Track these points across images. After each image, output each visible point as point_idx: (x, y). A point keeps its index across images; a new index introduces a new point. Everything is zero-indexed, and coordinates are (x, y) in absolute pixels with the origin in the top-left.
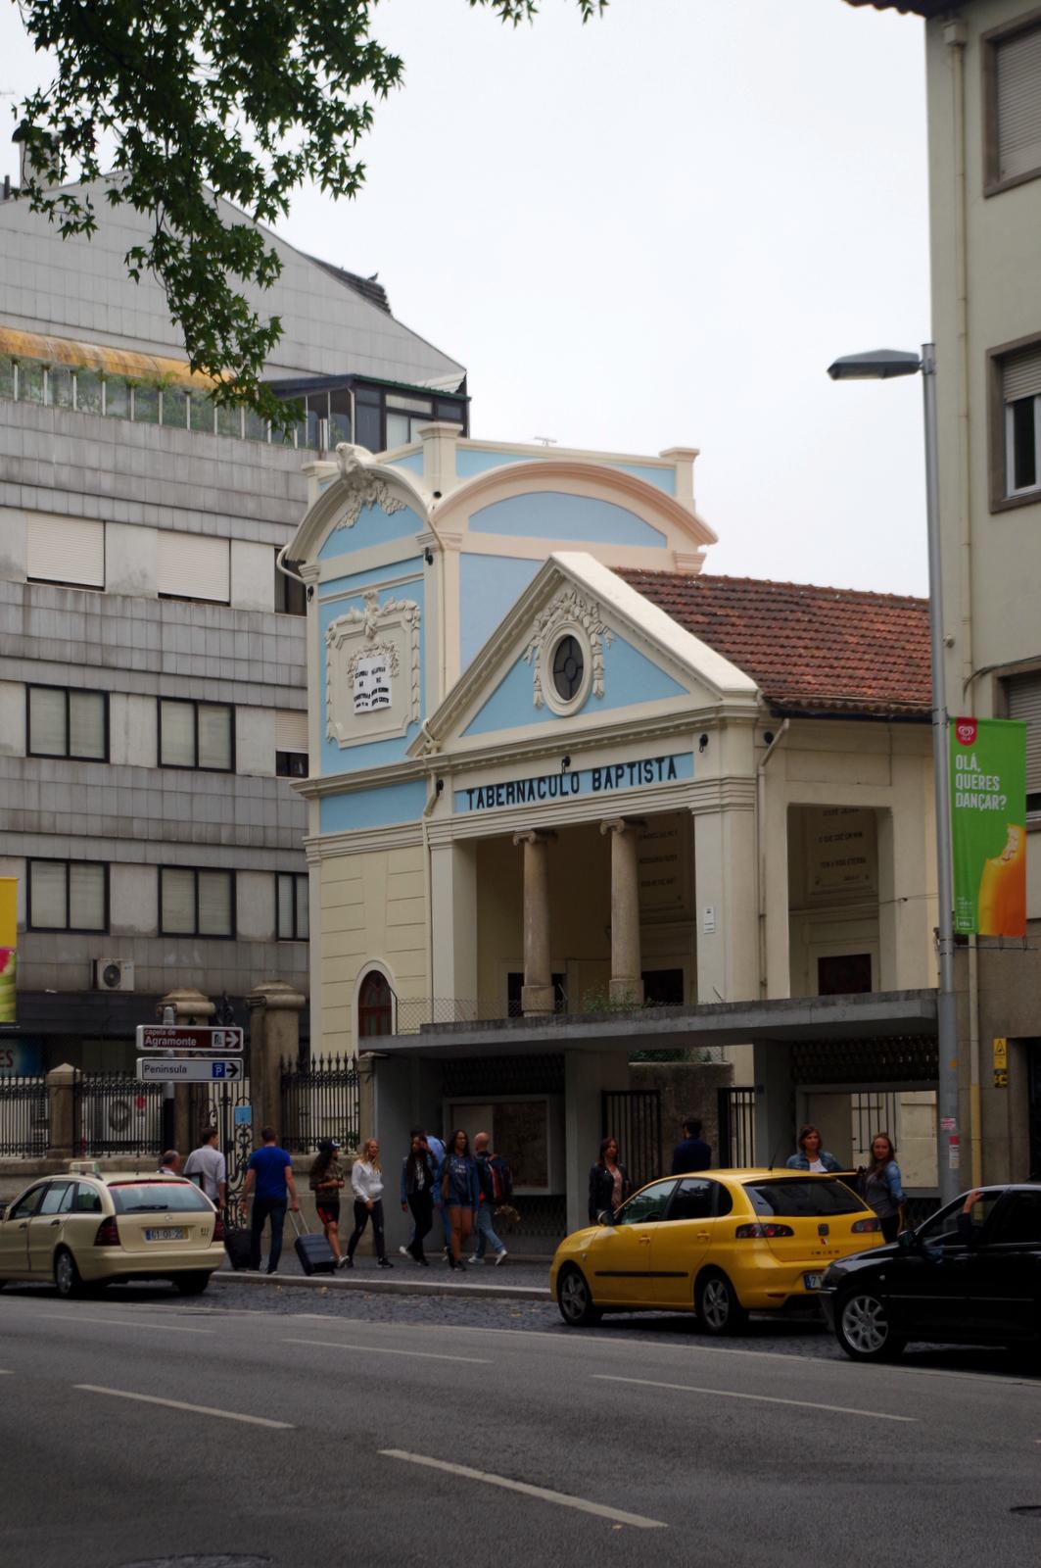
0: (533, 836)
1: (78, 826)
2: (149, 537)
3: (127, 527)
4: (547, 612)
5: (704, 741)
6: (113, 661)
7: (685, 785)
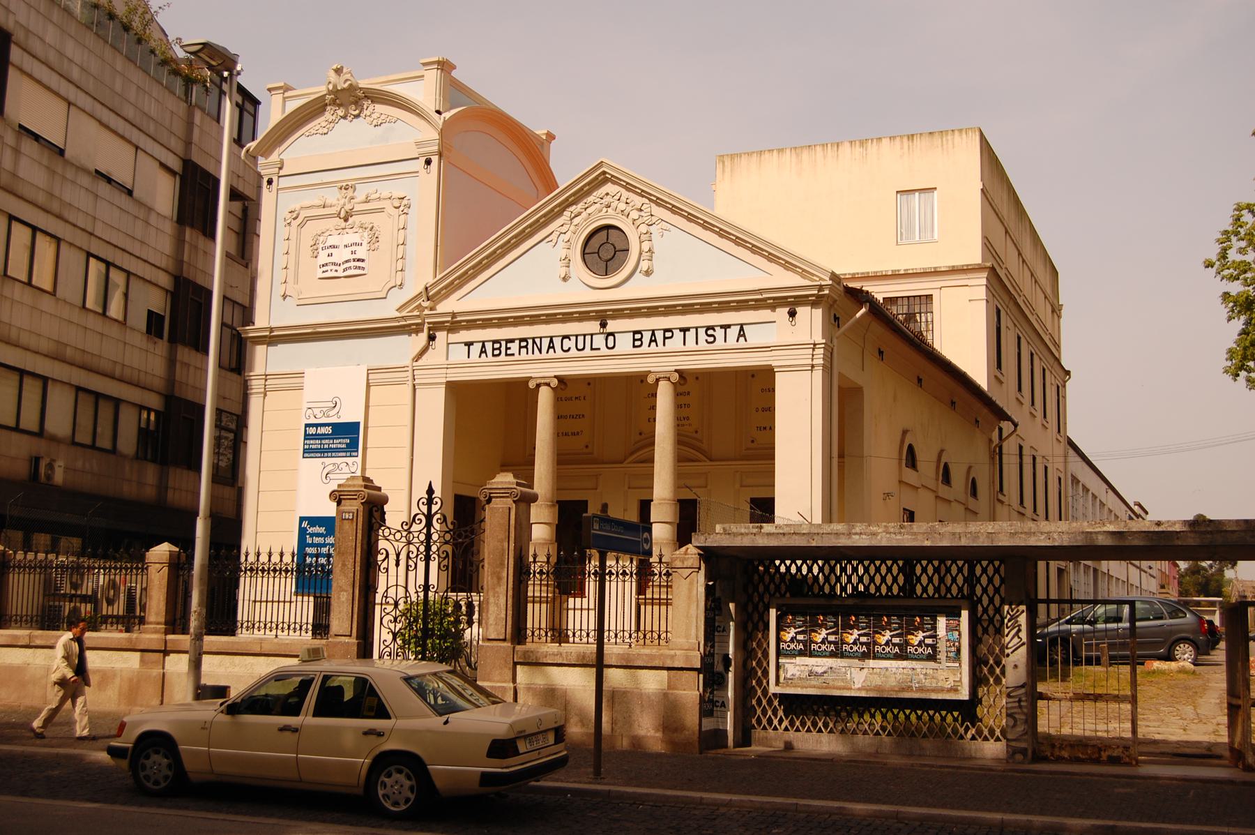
0: (555, 383)
1: (33, 342)
2: (93, 125)
3: (82, 113)
4: (581, 205)
5: (792, 314)
6: (66, 214)
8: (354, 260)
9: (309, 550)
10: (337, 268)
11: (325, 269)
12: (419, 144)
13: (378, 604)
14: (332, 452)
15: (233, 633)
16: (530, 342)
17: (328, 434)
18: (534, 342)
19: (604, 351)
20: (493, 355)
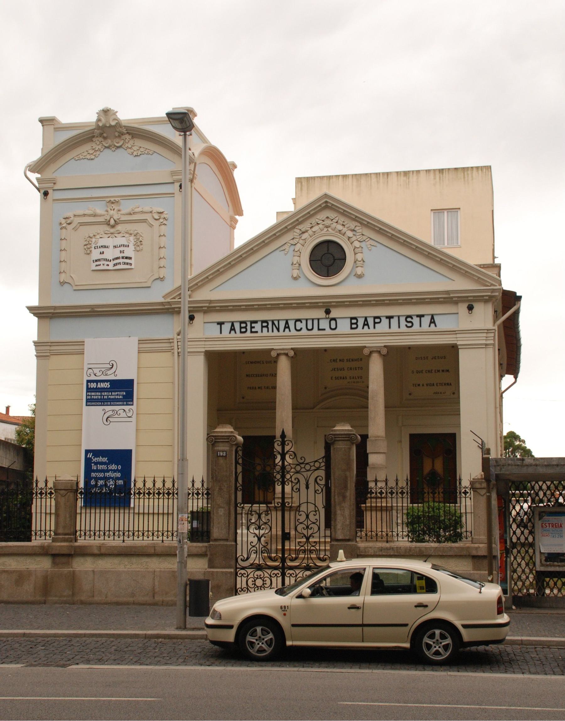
5: (470, 308)
7: (455, 331)
8: (123, 258)
9: (93, 475)
10: (108, 263)
11: (98, 263)
12: (173, 173)
13: (53, 513)
14: (111, 402)
15: (29, 540)
16: (270, 323)
17: (107, 388)
18: (273, 323)
19: (328, 331)
20: (241, 332)
